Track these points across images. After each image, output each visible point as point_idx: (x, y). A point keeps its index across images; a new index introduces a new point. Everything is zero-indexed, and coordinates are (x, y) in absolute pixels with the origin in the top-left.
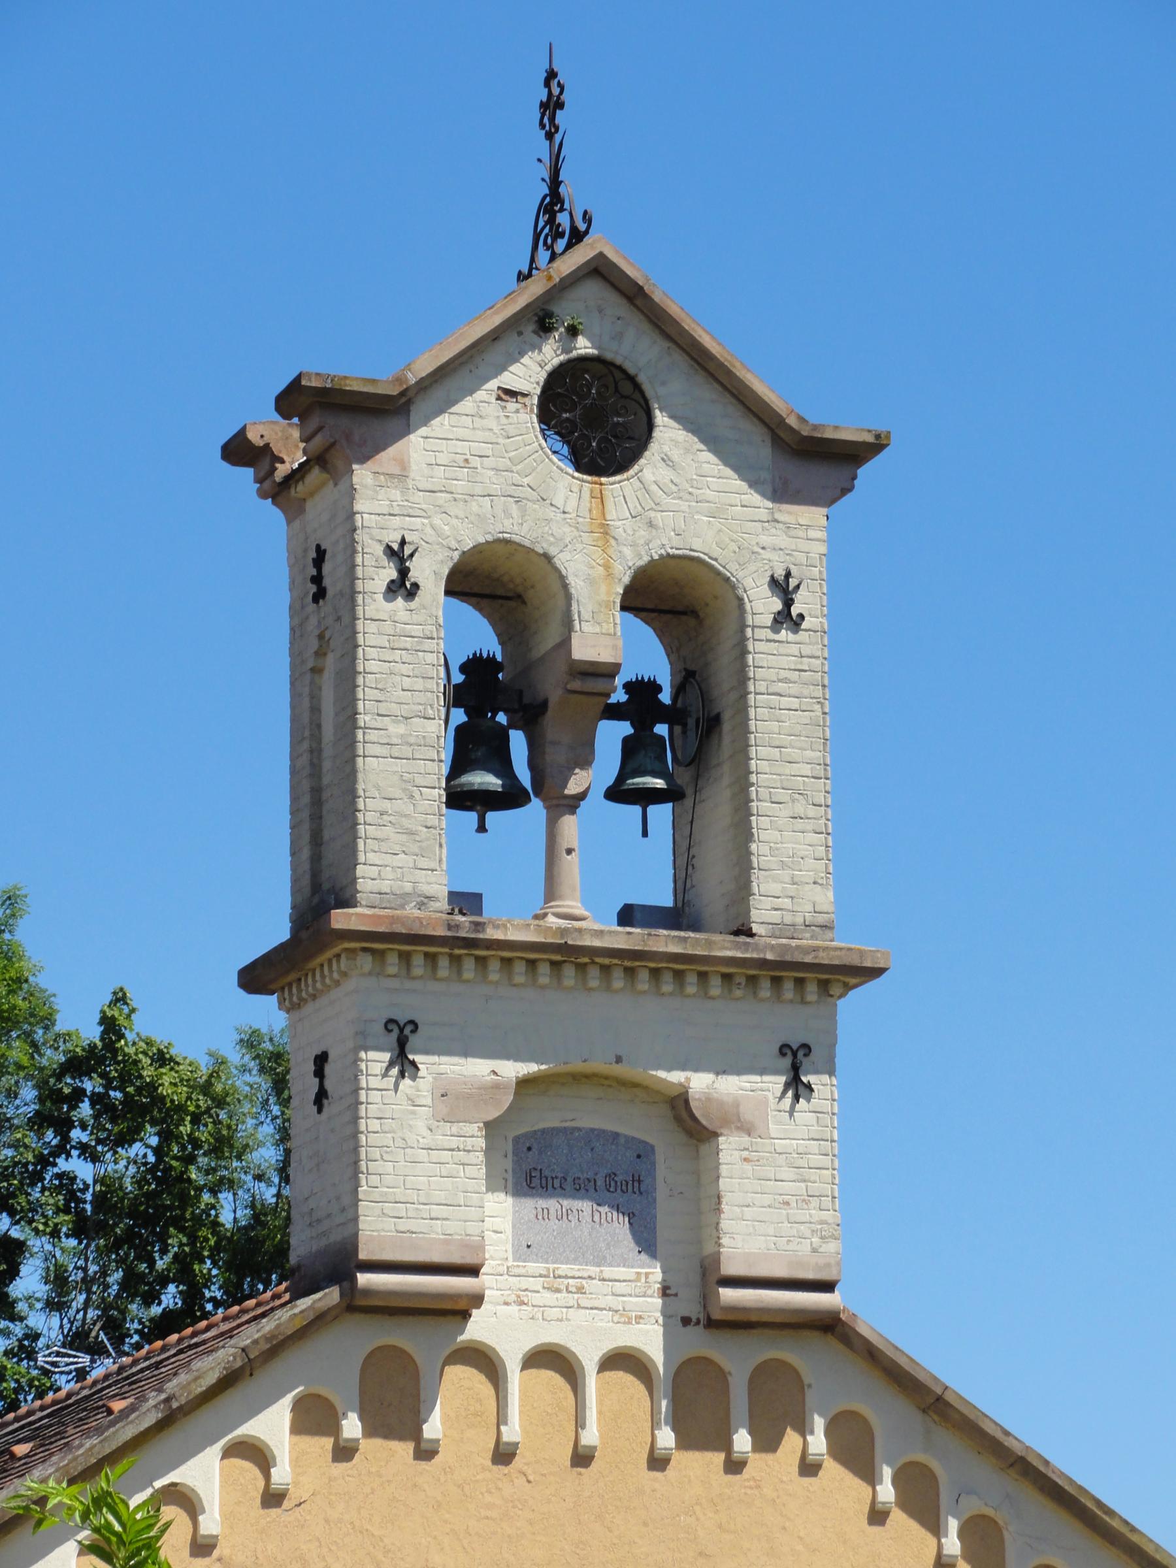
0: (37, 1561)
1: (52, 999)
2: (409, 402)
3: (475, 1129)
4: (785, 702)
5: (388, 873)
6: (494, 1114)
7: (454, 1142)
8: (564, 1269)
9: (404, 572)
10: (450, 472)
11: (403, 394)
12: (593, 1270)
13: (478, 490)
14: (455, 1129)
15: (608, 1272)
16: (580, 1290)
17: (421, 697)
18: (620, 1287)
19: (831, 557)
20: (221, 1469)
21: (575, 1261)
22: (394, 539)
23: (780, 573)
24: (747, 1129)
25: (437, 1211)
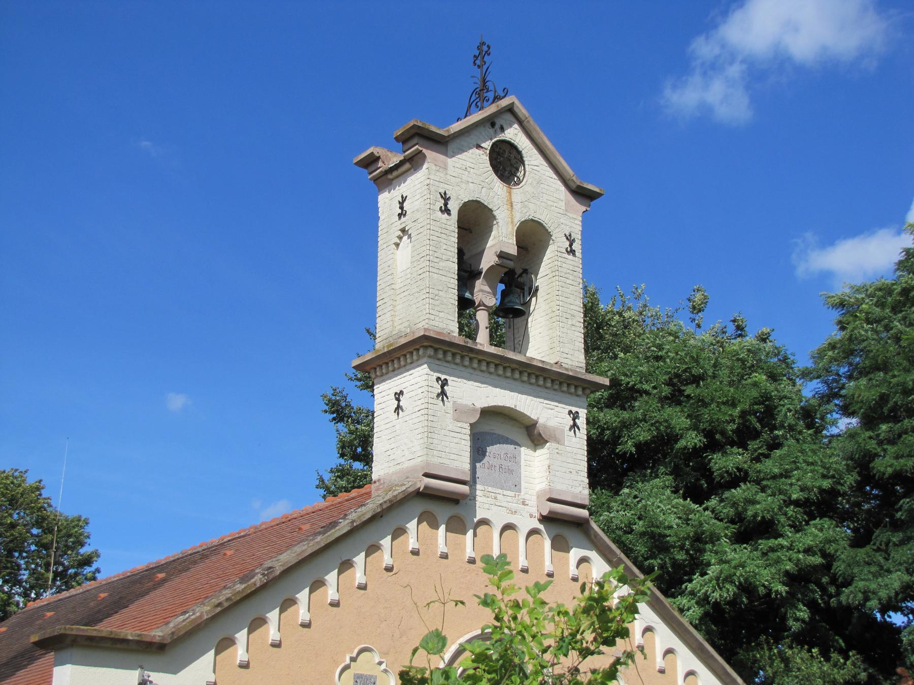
0: (198, 658)
1: (327, 408)
2: (447, 142)
3: (467, 426)
4: (568, 281)
5: (437, 319)
6: (473, 421)
7: (459, 430)
8: (490, 489)
9: (446, 205)
10: (460, 171)
11: (449, 136)
12: (500, 491)
13: (470, 180)
14: (460, 424)
15: (506, 492)
16: (496, 498)
17: (449, 253)
18: (509, 499)
19: (583, 233)
20: (492, 549)
21: (493, 486)
22: (442, 191)
23: (568, 234)
24: (558, 442)
25: (452, 457)
